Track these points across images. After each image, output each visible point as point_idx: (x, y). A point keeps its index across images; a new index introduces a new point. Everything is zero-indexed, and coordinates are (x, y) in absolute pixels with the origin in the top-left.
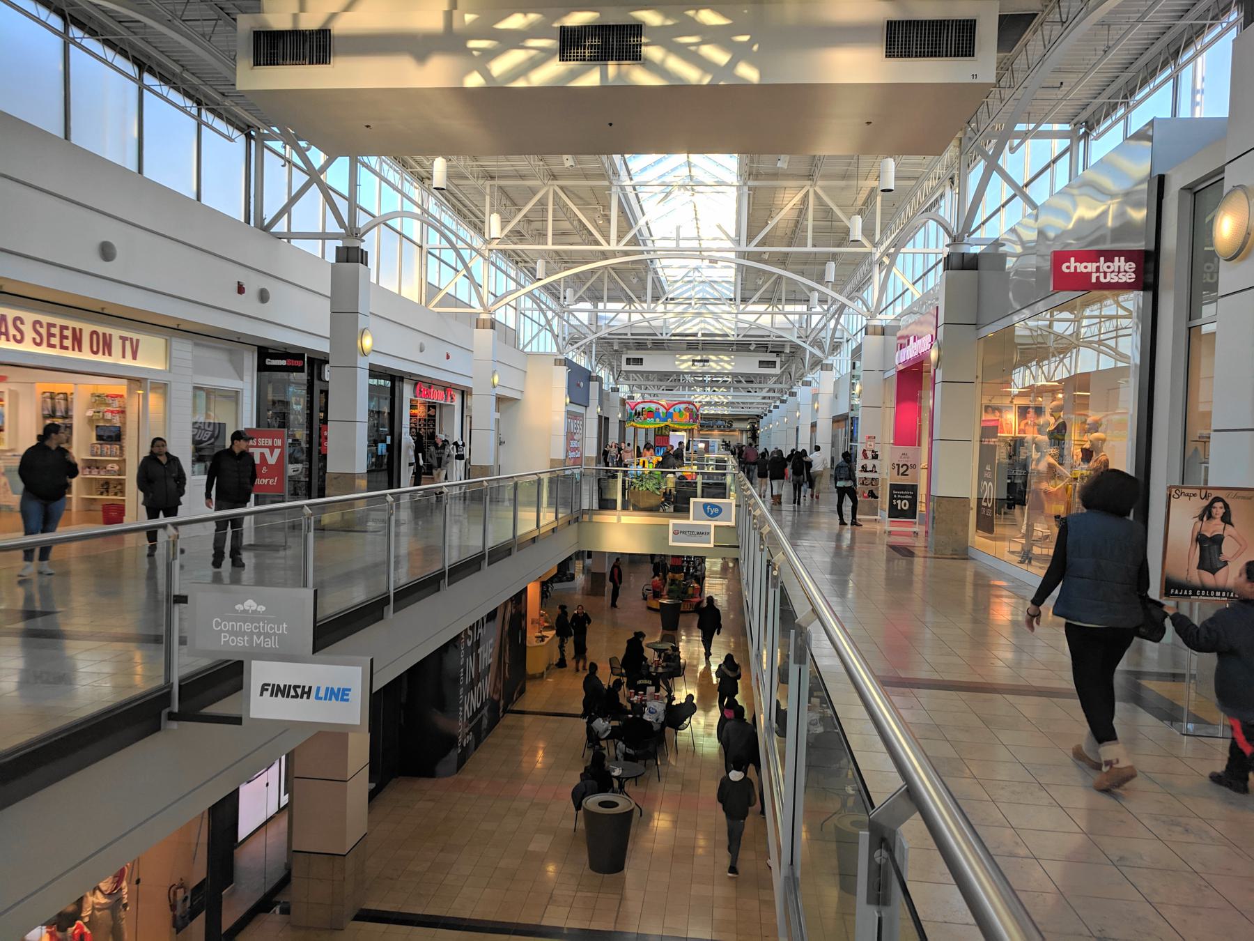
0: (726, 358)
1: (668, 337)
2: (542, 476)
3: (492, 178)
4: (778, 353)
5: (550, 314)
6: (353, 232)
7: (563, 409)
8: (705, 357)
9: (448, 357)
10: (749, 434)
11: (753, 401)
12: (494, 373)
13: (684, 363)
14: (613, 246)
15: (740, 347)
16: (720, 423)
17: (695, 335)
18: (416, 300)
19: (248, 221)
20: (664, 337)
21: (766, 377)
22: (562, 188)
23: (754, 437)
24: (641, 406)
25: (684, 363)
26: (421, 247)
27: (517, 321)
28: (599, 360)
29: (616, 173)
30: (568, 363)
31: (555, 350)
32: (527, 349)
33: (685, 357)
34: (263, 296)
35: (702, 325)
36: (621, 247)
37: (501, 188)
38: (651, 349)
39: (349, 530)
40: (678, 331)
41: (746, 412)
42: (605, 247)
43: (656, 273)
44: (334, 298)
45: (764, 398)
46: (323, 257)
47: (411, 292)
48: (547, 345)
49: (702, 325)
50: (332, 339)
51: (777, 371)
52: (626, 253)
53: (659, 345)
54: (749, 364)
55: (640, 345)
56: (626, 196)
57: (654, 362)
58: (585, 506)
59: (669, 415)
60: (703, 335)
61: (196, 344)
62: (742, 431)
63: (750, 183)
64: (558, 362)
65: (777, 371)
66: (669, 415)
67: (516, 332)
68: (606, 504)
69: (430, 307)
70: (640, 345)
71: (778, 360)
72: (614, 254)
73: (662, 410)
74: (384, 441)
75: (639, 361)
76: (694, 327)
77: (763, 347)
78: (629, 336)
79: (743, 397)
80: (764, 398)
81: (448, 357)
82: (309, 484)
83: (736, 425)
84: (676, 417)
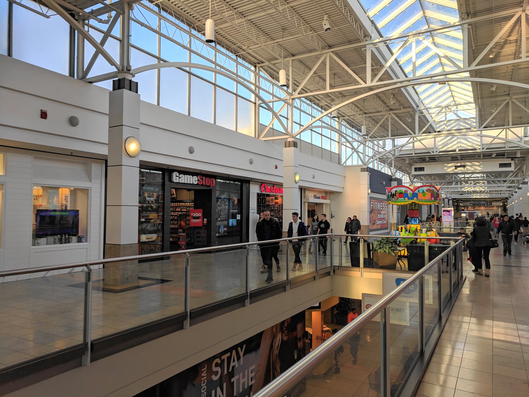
0: (477, 164)
1: (437, 153)
2: (92, 267)
3: (293, 55)
4: (512, 159)
5: (355, 144)
6: (125, 68)
7: (366, 196)
8: (463, 164)
9: (276, 167)
10: (502, 208)
11: (502, 189)
12: (295, 174)
13: (450, 168)
14: (369, 84)
15: (486, 155)
16: (482, 202)
17: (455, 151)
18: (253, 136)
19: (72, 74)
20: (435, 153)
21: (507, 173)
22: (336, 54)
23: (505, 209)
24: (395, 189)
25: (450, 168)
26: (255, 104)
27: (340, 149)
28: (400, 169)
29: (367, 35)
30: (369, 170)
31: (360, 163)
32: (349, 163)
33: (450, 165)
34: (73, 122)
35: (459, 145)
36: (375, 83)
37: (300, 61)
38: (428, 162)
39: (162, 280)
40: (443, 149)
41: (498, 196)
42: (363, 85)
43: (422, 113)
44: (111, 115)
45: (509, 187)
46: (158, 104)
47: (247, 129)
48: (355, 161)
49: (459, 145)
50: (109, 145)
51: (512, 168)
52: (378, 87)
53: (433, 159)
54: (494, 166)
55: (423, 160)
56: (378, 49)
57: (430, 169)
58: (336, 263)
59: (415, 195)
60: (460, 150)
61: (35, 158)
62: (498, 207)
63: (470, 20)
64: (363, 170)
65: (512, 168)
66: (415, 195)
67: (339, 156)
68: (355, 263)
69: (261, 138)
70: (423, 160)
71: (513, 163)
72: (371, 89)
73: (410, 192)
74: (235, 218)
75: (422, 169)
76: (456, 145)
77: (501, 155)
78: (414, 155)
79: (495, 187)
80: (509, 187)
81: (276, 167)
82: (162, 246)
83: (494, 204)
84: (420, 196)
